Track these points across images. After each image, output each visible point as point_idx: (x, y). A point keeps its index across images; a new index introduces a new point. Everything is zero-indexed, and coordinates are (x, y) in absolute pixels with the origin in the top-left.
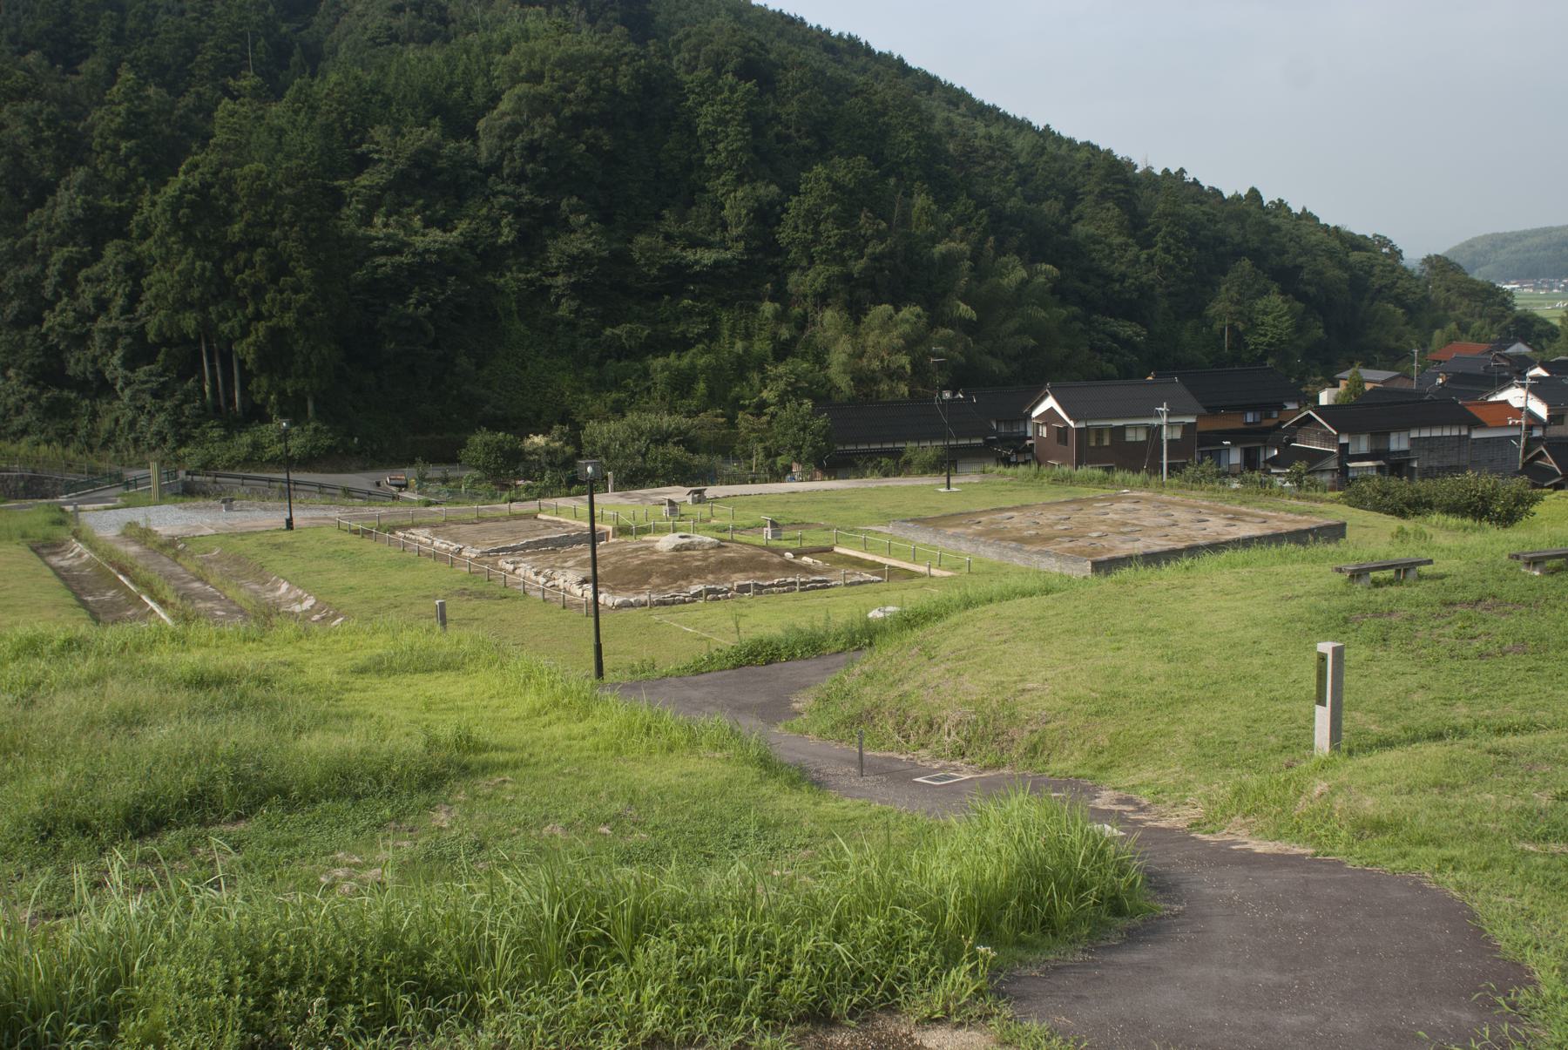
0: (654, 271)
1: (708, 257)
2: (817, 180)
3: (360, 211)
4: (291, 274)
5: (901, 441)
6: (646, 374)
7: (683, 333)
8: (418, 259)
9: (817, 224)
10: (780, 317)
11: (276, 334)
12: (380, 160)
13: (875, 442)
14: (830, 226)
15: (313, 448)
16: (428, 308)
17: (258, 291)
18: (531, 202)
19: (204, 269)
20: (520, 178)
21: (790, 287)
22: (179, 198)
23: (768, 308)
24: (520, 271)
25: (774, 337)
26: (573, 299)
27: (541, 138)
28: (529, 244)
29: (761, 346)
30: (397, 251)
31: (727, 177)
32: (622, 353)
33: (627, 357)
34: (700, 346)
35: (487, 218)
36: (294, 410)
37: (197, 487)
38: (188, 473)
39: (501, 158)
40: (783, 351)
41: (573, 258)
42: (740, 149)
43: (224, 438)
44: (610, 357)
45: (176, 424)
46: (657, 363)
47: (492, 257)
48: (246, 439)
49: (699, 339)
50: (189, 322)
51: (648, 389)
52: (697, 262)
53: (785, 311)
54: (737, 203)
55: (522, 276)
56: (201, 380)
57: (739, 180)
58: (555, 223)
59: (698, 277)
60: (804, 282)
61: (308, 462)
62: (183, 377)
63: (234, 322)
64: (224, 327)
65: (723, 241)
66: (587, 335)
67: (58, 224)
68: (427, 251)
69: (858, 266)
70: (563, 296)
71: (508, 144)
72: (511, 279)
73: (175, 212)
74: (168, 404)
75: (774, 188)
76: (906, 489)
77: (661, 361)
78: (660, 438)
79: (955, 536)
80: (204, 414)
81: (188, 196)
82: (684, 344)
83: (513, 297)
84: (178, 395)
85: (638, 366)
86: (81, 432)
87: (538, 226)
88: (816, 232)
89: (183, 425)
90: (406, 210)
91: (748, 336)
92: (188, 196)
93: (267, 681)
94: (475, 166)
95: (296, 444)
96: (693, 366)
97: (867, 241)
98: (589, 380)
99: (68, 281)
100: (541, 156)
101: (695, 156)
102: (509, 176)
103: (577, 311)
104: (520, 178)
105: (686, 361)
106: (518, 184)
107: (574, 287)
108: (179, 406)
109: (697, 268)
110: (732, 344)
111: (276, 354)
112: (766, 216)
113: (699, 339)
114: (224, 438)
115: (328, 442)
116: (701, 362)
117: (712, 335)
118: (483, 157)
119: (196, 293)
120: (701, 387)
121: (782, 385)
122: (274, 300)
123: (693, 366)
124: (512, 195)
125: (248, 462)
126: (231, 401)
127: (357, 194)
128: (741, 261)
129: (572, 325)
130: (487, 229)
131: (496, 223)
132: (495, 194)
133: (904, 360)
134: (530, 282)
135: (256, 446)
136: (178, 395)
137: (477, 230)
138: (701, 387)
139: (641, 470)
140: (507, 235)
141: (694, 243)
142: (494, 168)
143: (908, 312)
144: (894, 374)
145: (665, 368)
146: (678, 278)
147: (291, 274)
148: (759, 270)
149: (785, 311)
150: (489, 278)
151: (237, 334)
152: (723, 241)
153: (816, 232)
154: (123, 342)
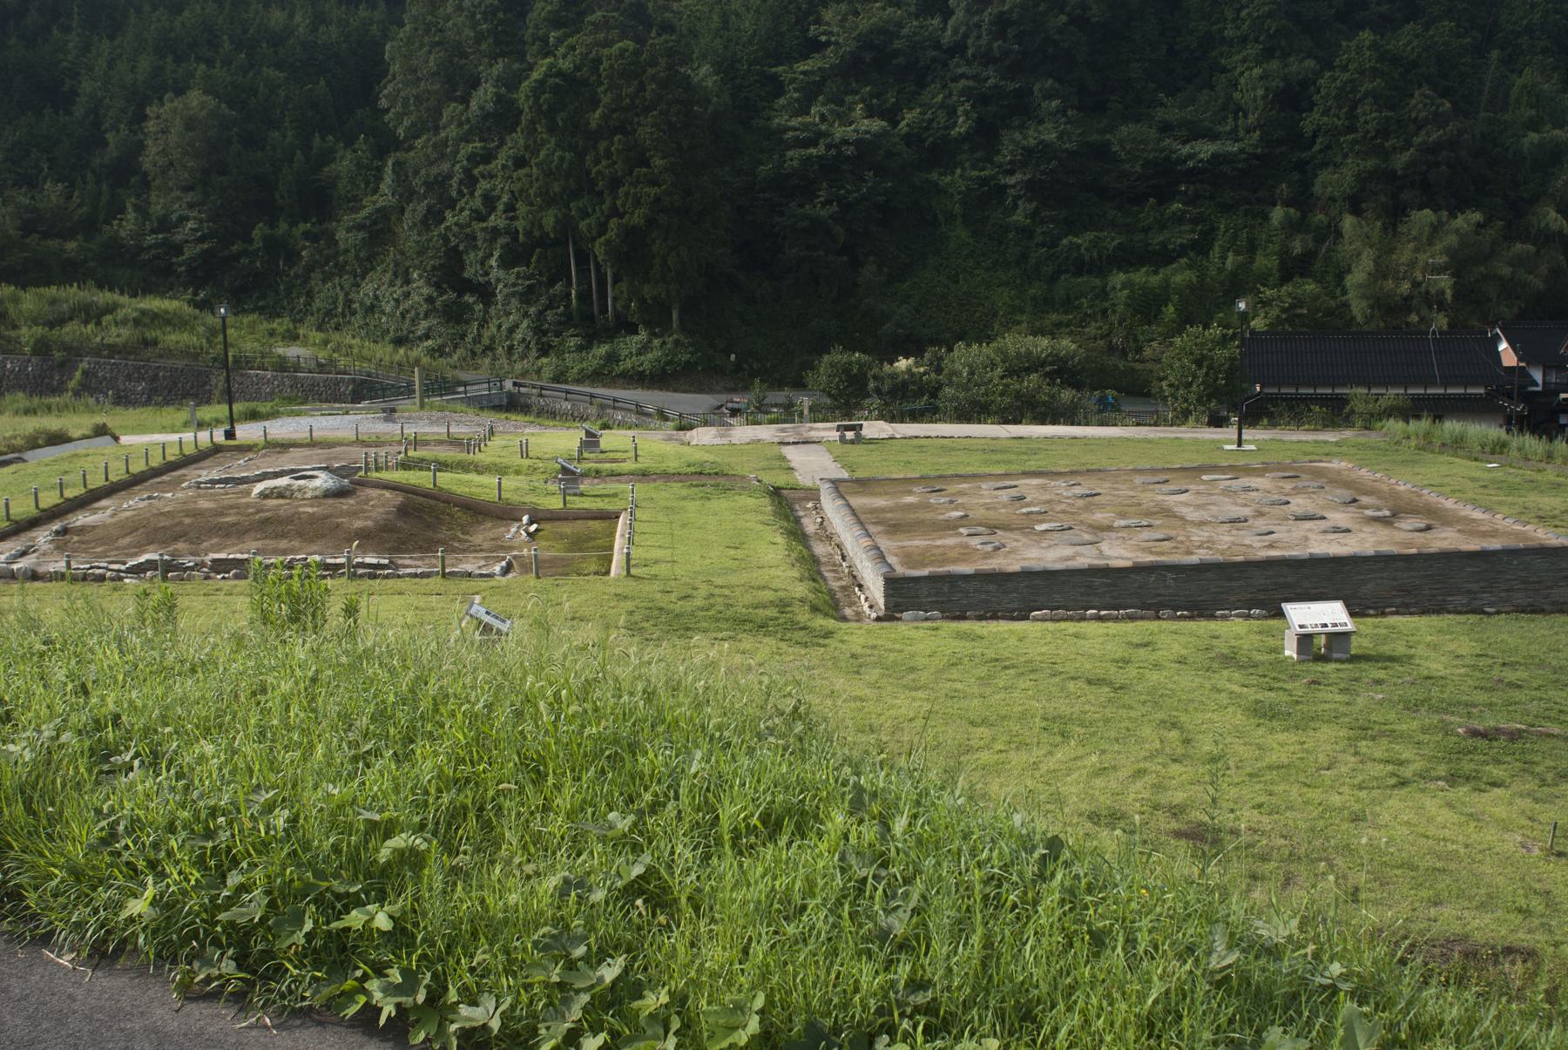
0: (1138, 168)
1: (1205, 149)
2: (1359, 49)
3: (797, 100)
4: (648, 165)
5: (1344, 385)
6: (1104, 294)
7: (1164, 245)
8: (833, 152)
9: (1353, 108)
10: (1292, 227)
11: (630, 233)
12: (828, 44)
13: (1324, 385)
14: (1367, 108)
15: (667, 363)
16: (835, 208)
17: (615, 183)
18: (996, 86)
19: (562, 159)
20: (987, 59)
21: (1317, 189)
22: (542, 82)
23: (1277, 214)
24: (974, 167)
25: (1284, 253)
26: (1030, 200)
27: (1011, 11)
28: (986, 134)
29: (1265, 261)
30: (813, 143)
31: (1252, 50)
32: (1081, 267)
33: (1090, 272)
34: (1184, 261)
35: (942, 106)
36: (656, 319)
37: (522, 400)
38: (515, 384)
39: (966, 36)
40: (1292, 269)
41: (1029, 151)
42: (1269, 15)
43: (580, 348)
44: (1066, 271)
45: (539, 331)
46: (1118, 278)
47: (940, 153)
48: (603, 350)
49: (1182, 251)
50: (549, 220)
51: (1104, 311)
52: (1191, 156)
53: (1304, 217)
54: (1252, 81)
55: (975, 173)
56: (569, 283)
57: (1268, 54)
58: (1021, 108)
59: (1192, 175)
60: (1332, 181)
61: (659, 379)
62: (552, 282)
63: (591, 220)
64: (583, 225)
65: (1235, 131)
66: (1043, 245)
67: (468, 120)
68: (845, 142)
69: (1401, 160)
70: (1020, 197)
71: (976, 18)
72: (957, 180)
73: (537, 98)
74: (532, 310)
75: (1310, 63)
76: (1110, 442)
77: (1122, 277)
78: (1031, 364)
79: (1494, 533)
80: (567, 321)
81: (551, 81)
82: (1162, 258)
83: (957, 198)
84: (543, 300)
85: (1098, 282)
86: (469, 338)
87: (999, 114)
88: (1352, 115)
89: (545, 333)
90: (849, 99)
91: (1252, 248)
92: (551, 81)
93: (540, 624)
94: (937, 45)
95: (648, 361)
96: (1166, 286)
97: (1420, 128)
98: (1034, 298)
99: (470, 181)
100: (1011, 32)
101: (1215, 28)
102: (974, 56)
103: (1034, 215)
104: (987, 59)
105: (1155, 280)
106: (986, 65)
107: (1030, 185)
108: (541, 313)
109: (1191, 164)
110: (1224, 258)
111: (633, 255)
112: (1293, 98)
113: (1182, 251)
114: (580, 348)
115: (685, 357)
116: (1178, 279)
117: (1201, 247)
118: (947, 38)
119: (556, 187)
120: (1170, 310)
121: (1274, 312)
122: (627, 194)
123: (1166, 286)
124: (975, 78)
125: (597, 377)
126: (604, 310)
127: (793, 80)
128: (1256, 157)
129: (1027, 233)
130: (942, 118)
131: (952, 113)
132: (955, 79)
133: (1445, 282)
134: (984, 182)
135: (612, 358)
136: (543, 300)
137: (931, 121)
138: (1170, 310)
139: (974, 403)
140: (962, 127)
141: (1197, 133)
142: (958, 48)
143: (1467, 220)
144: (1435, 301)
145: (1126, 285)
146: (1165, 178)
147: (648, 165)
148: (1279, 162)
149: (1304, 217)
150: (934, 176)
151: (594, 232)
152: (1235, 131)
153: (1352, 115)
154: (502, 241)
